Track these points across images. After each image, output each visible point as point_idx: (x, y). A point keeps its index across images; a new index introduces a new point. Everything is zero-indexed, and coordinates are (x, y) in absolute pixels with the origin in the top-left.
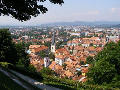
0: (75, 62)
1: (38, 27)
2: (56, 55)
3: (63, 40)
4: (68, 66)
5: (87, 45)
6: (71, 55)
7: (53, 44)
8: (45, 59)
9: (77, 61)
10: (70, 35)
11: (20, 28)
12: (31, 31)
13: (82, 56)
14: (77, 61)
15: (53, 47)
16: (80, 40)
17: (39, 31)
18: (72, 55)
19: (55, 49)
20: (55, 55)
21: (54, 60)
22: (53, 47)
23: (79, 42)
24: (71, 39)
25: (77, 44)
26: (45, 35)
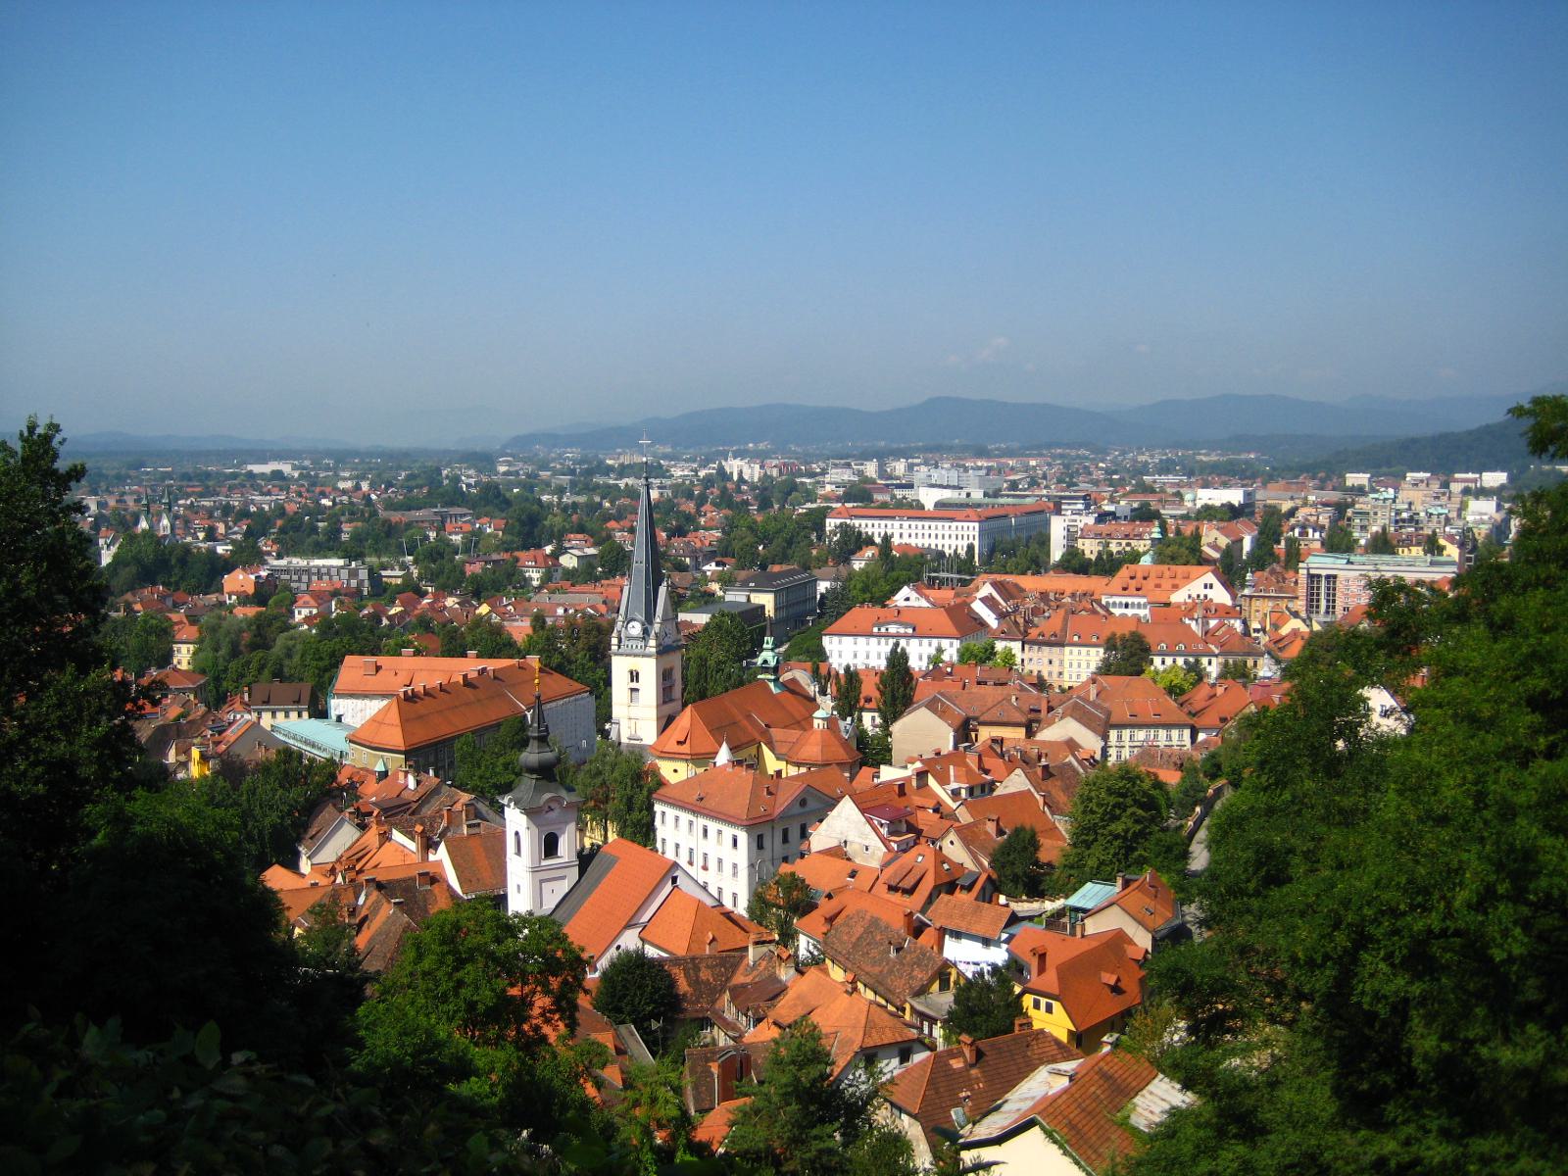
0: (920, 857)
1: (483, 460)
2: (674, 772)
3: (99, 840)
4: (826, 907)
5: (1071, 654)
6: (866, 771)
7: (636, 629)
8: (515, 820)
9: (955, 850)
10: (862, 541)
11: (257, 469)
12: (391, 506)
13: (1016, 782)
14: (955, 850)
15: (634, 676)
16: (988, 601)
17: (491, 498)
18: (887, 774)
19: (665, 694)
20: (655, 772)
21: (643, 832)
22: (634, 676)
23: (966, 623)
24: (876, 590)
25: (951, 650)
26: (560, 551)
